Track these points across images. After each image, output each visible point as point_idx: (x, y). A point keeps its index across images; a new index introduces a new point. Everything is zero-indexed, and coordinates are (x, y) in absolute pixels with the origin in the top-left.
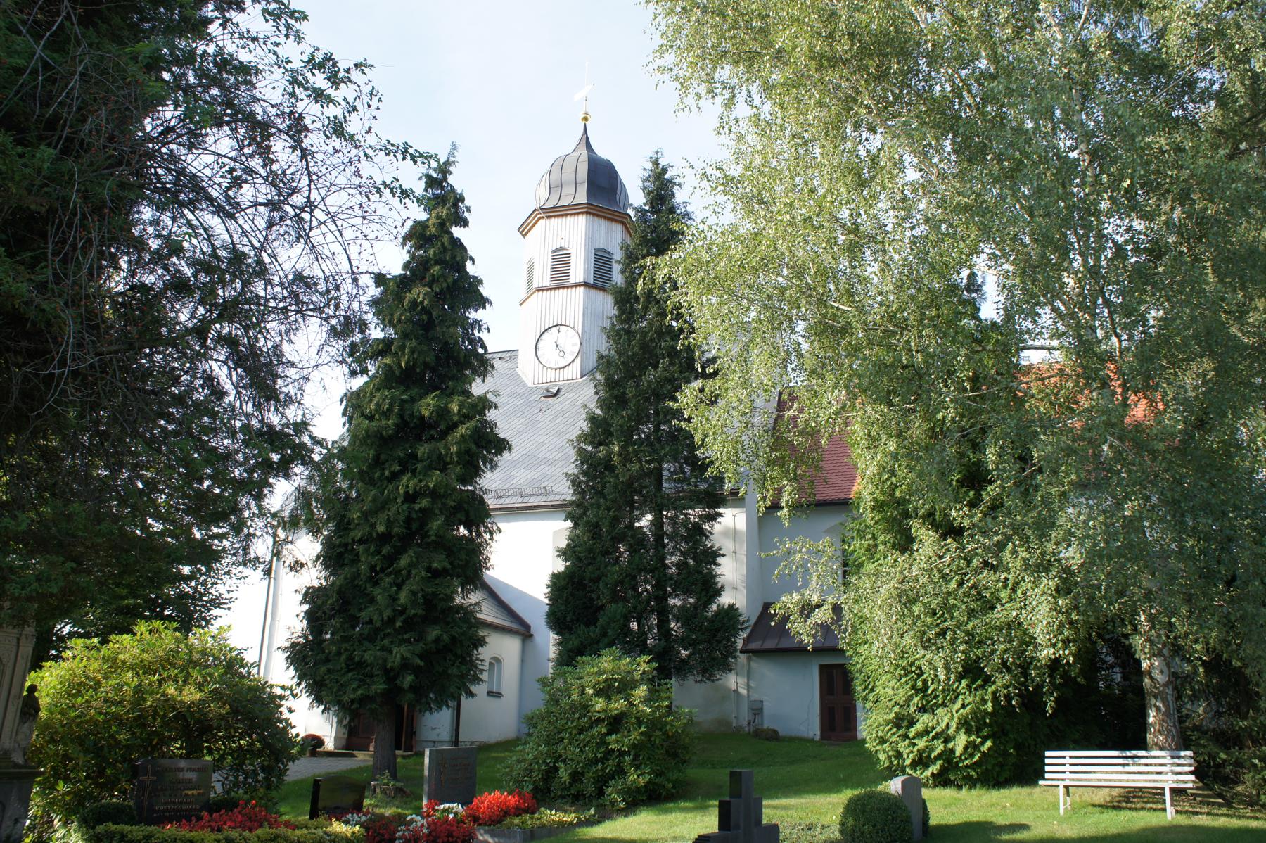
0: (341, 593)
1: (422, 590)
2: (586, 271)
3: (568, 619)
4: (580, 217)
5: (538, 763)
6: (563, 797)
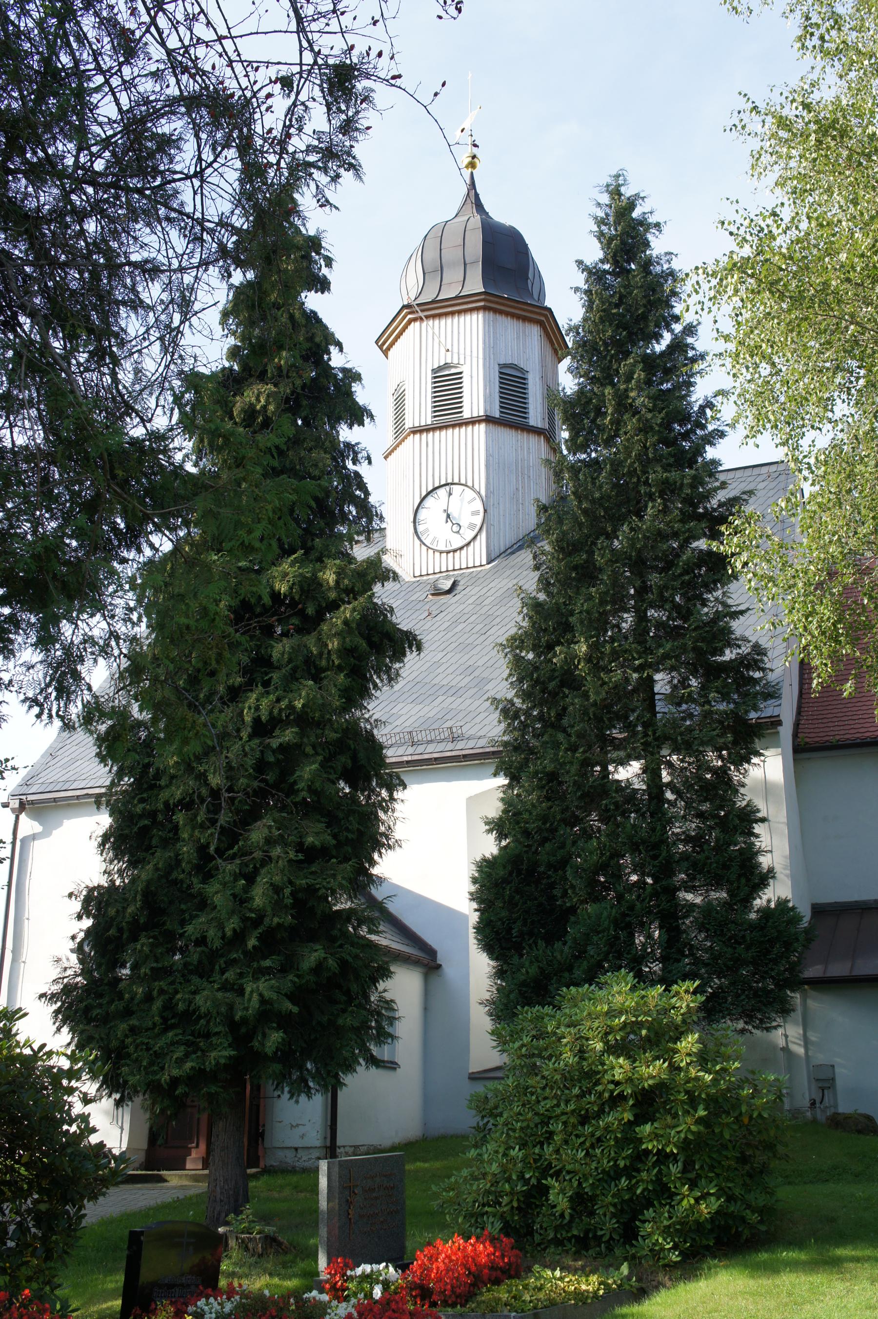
0: (149, 896)
1: (290, 882)
2: (487, 399)
3: (515, 932)
4: (474, 316)
5: (508, 1180)
6: (558, 1242)
